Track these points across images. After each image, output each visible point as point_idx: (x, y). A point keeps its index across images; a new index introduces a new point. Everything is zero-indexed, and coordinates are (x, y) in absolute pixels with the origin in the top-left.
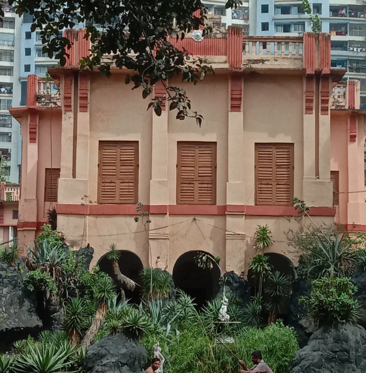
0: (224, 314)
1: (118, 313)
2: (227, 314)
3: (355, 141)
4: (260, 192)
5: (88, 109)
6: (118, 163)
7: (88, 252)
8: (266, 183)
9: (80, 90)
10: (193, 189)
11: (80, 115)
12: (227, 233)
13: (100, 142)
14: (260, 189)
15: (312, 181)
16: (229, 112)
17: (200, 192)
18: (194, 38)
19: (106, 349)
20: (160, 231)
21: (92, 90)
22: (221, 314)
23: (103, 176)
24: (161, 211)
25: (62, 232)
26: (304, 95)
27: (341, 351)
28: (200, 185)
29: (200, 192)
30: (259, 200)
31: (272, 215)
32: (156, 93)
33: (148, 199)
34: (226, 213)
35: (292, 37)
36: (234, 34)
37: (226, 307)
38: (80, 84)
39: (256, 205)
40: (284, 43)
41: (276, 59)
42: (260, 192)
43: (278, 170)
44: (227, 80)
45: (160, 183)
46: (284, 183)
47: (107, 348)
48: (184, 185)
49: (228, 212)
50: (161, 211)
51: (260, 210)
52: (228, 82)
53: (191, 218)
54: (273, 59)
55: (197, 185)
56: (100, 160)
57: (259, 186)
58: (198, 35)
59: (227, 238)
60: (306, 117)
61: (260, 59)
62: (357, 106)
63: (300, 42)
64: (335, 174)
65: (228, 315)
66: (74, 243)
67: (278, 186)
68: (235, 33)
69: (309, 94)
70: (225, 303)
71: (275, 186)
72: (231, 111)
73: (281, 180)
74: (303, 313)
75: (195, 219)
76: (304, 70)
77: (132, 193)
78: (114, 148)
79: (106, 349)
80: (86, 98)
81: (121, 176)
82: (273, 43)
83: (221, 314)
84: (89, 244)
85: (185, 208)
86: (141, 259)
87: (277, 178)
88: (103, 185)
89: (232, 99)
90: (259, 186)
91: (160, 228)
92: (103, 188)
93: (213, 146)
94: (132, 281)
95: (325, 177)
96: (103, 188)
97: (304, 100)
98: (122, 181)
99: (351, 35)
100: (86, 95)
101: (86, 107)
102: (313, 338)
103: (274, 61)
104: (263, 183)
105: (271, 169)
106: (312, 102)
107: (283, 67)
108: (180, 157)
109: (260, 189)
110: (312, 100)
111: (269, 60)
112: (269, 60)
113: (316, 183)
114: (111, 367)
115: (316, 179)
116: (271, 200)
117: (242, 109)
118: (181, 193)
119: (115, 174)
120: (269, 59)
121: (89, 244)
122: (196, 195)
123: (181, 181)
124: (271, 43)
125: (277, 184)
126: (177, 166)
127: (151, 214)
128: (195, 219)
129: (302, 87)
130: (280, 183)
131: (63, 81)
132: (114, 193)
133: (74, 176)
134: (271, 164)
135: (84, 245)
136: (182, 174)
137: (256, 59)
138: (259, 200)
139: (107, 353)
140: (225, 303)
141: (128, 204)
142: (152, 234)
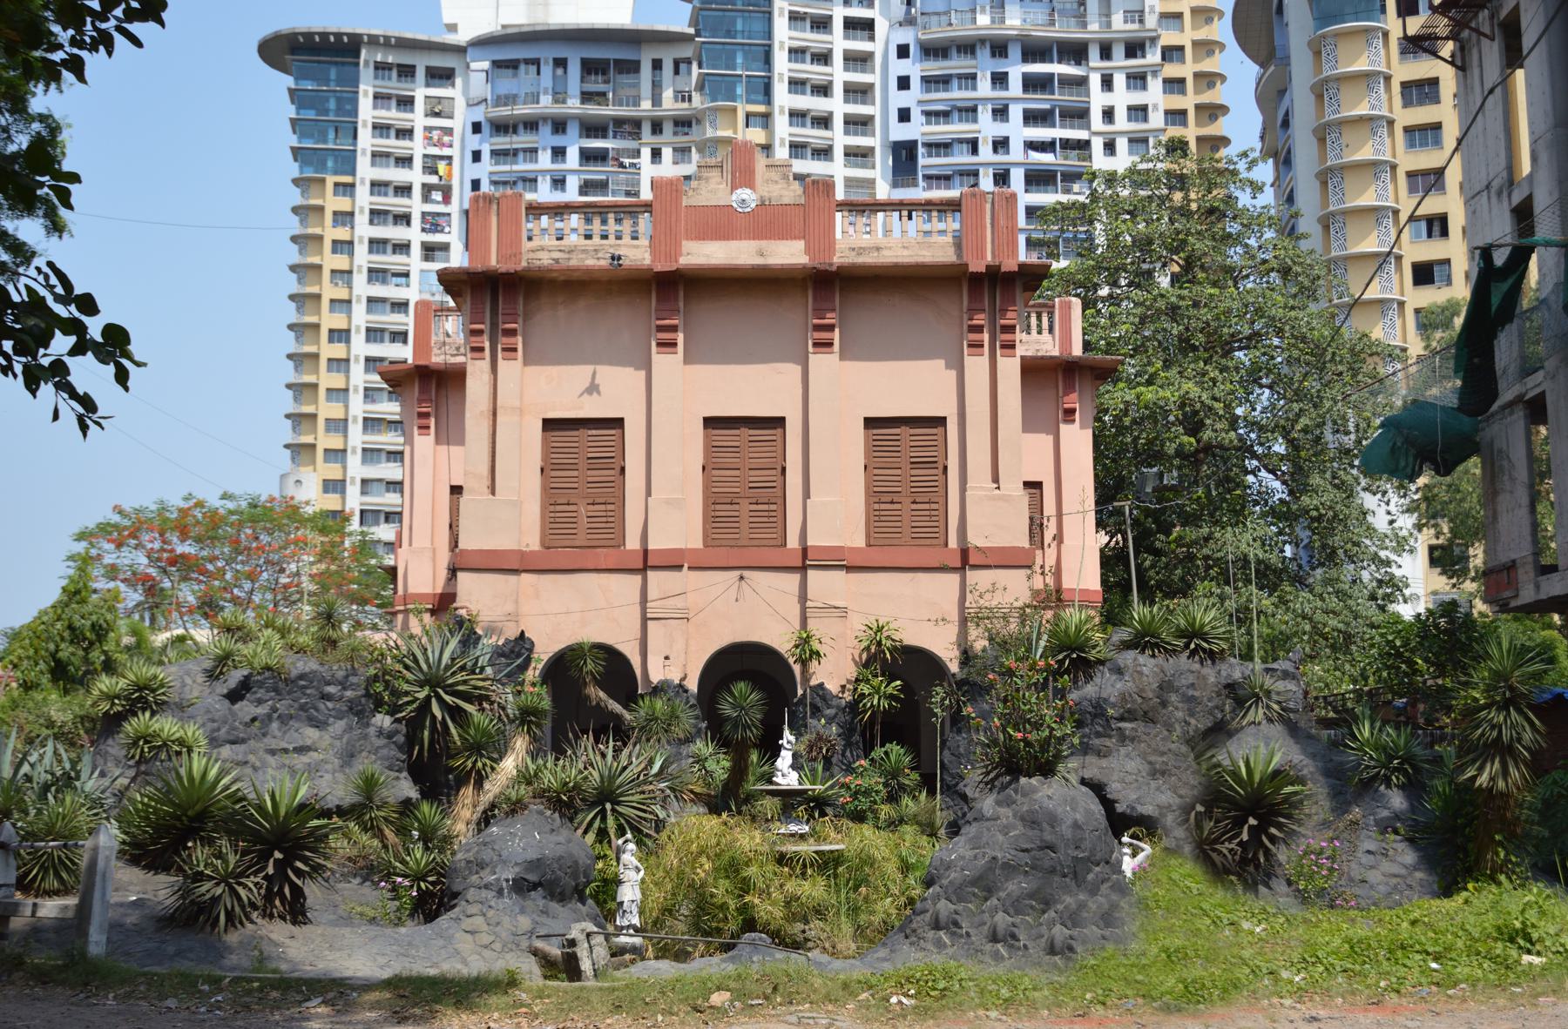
0: (785, 771)
3: (1074, 421)
6: (583, 464)
7: (520, 648)
11: (502, 365)
17: (752, 520)
18: (735, 205)
19: (493, 849)
20: (671, 602)
24: (672, 561)
25: (468, 605)
27: (1041, 848)
29: (752, 520)
31: (800, 391)
38: (504, 304)
39: (868, 545)
43: (914, 472)
44: (805, 290)
45: (668, 502)
47: (496, 847)
48: (718, 507)
50: (672, 561)
51: (877, 557)
52: (806, 290)
53: (737, 573)
55: (745, 507)
56: (545, 457)
57: (876, 506)
62: (1077, 350)
64: (1034, 486)
66: (490, 631)
67: (914, 506)
70: (788, 746)
71: (907, 505)
74: (972, 765)
75: (742, 578)
79: (493, 849)
84: (523, 632)
85: (720, 556)
88: (552, 508)
90: (876, 506)
95: (1013, 486)
99: (1063, 126)
104: (883, 500)
108: (710, 449)
111: (890, 248)
113: (993, 498)
114: (500, 892)
118: (712, 520)
121: (523, 632)
122: (745, 526)
123: (712, 501)
126: (704, 468)
128: (742, 578)
129: (961, 296)
131: (468, 299)
133: (493, 493)
135: (512, 634)
139: (495, 858)
140: (788, 746)
142: (653, 609)
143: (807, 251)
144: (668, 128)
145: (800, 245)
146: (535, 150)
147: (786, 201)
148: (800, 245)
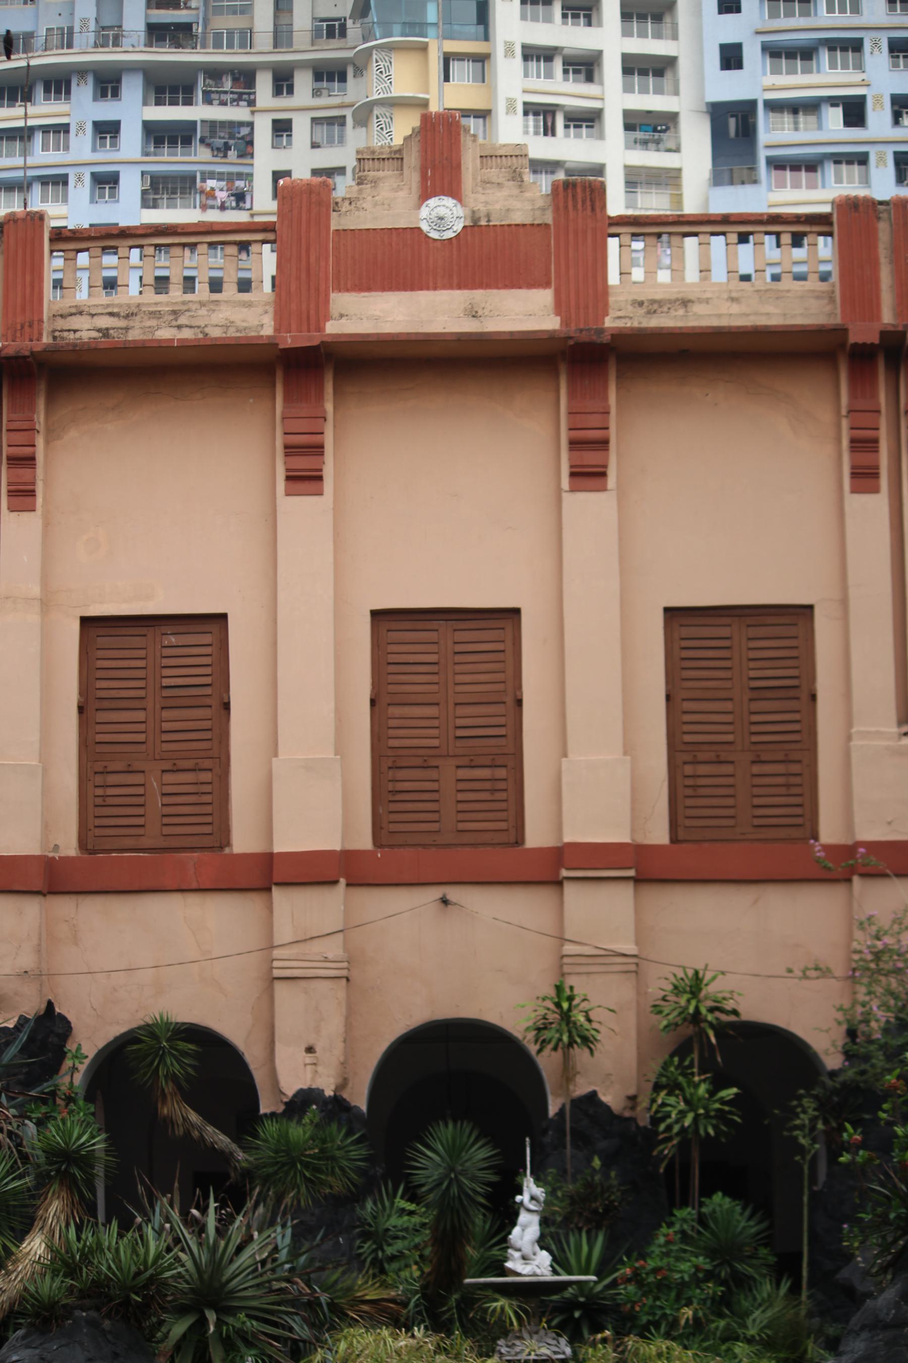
1: (708, 1260)
2: (542, 1248)
4: (689, 792)
5: (39, 500)
8: (711, 756)
9: (8, 430)
10: (434, 786)
12: (569, 949)
13: (87, 622)
14: (689, 782)
15: (885, 743)
16: (564, 495)
21: (51, 435)
22: (519, 1250)
23: (99, 748)
26: (845, 423)
28: (463, 773)
30: (688, 823)
32: (852, 428)
33: (849, 825)
34: (564, 873)
35: (136, 228)
36: (575, 206)
37: (536, 1219)
39: (674, 839)
40: (206, 246)
41: (734, 295)
42: (689, 792)
43: (755, 706)
46: (488, 763)
49: (568, 869)
54: (725, 296)
57: (688, 770)
58: (441, 218)
59: (566, 969)
60: (857, 503)
61: (673, 297)
63: (821, 234)
65: (545, 1253)
67: (756, 769)
68: (580, 205)
69: (19, 438)
72: (573, 490)
73: (118, 748)
76: (840, 332)
77: (208, 809)
78: (137, 642)
80: (30, 461)
81: (165, 747)
82: (722, 238)
83: (519, 1250)
86: (248, 1058)
87: (755, 739)
88: (99, 780)
89: (574, 444)
90: (688, 770)
91: (312, 938)
92: (99, 792)
93: (214, 627)
94: (222, 1137)
96: (99, 792)
97: (845, 443)
98: (167, 766)
100: (30, 449)
101: (32, 493)
102: (863, 1328)
103: (729, 304)
104: (701, 756)
105: (728, 706)
106: (876, 450)
107: (762, 321)
109: (689, 782)
110: (876, 441)
111: (707, 301)
112: (707, 301)
115: (900, 739)
116: (730, 822)
117: (612, 480)
119: (141, 737)
120: (708, 295)
124: (713, 239)
125: (754, 762)
127: (277, 884)
128: (445, 901)
130: (763, 758)
132: (140, 811)
134: (728, 684)
136: (392, 732)
137: (658, 297)
138: (688, 823)
141: (193, 849)
143: (559, 307)
144: (303, 82)
145: (544, 298)
146: (64, 129)
147: (518, 218)
148: (544, 298)
